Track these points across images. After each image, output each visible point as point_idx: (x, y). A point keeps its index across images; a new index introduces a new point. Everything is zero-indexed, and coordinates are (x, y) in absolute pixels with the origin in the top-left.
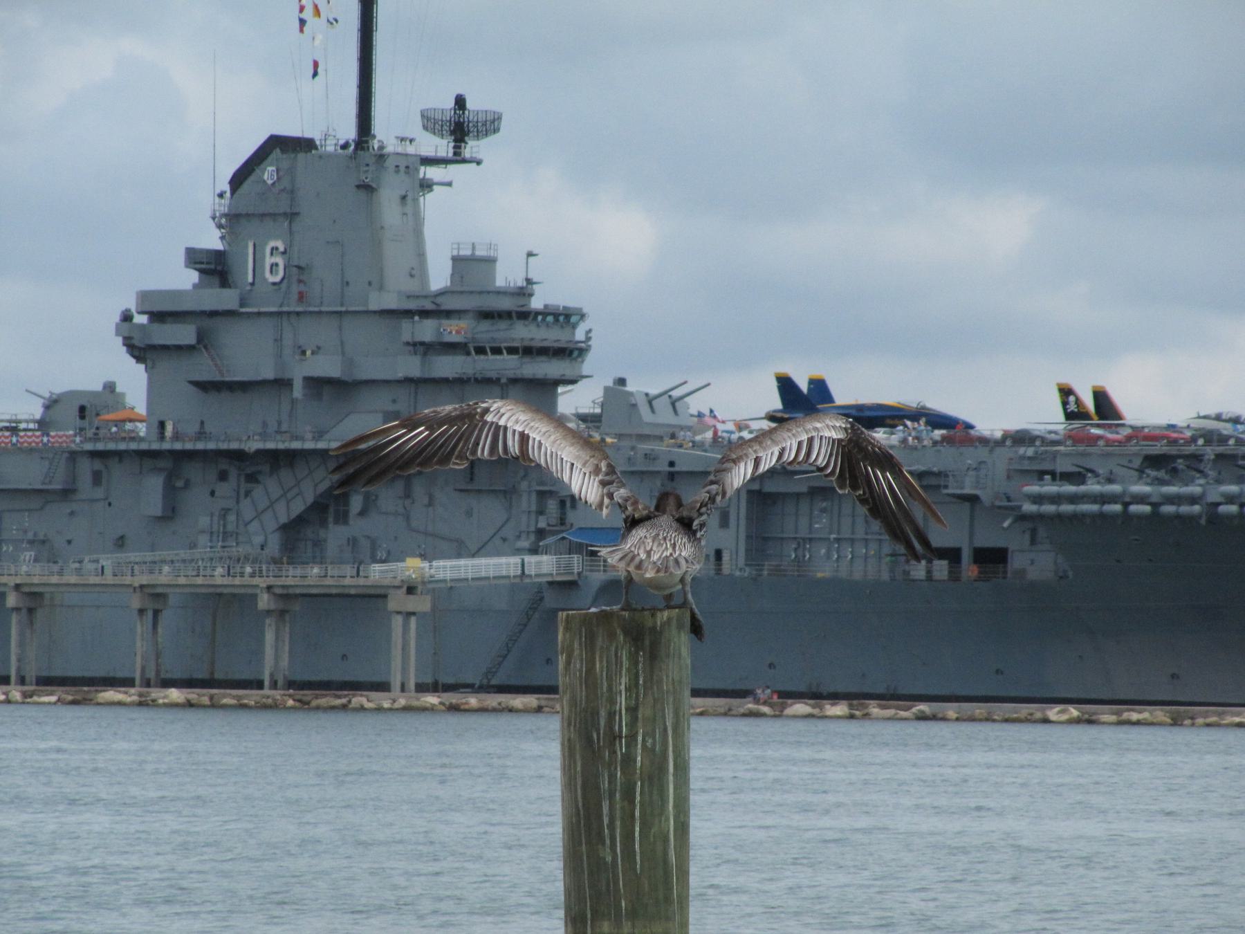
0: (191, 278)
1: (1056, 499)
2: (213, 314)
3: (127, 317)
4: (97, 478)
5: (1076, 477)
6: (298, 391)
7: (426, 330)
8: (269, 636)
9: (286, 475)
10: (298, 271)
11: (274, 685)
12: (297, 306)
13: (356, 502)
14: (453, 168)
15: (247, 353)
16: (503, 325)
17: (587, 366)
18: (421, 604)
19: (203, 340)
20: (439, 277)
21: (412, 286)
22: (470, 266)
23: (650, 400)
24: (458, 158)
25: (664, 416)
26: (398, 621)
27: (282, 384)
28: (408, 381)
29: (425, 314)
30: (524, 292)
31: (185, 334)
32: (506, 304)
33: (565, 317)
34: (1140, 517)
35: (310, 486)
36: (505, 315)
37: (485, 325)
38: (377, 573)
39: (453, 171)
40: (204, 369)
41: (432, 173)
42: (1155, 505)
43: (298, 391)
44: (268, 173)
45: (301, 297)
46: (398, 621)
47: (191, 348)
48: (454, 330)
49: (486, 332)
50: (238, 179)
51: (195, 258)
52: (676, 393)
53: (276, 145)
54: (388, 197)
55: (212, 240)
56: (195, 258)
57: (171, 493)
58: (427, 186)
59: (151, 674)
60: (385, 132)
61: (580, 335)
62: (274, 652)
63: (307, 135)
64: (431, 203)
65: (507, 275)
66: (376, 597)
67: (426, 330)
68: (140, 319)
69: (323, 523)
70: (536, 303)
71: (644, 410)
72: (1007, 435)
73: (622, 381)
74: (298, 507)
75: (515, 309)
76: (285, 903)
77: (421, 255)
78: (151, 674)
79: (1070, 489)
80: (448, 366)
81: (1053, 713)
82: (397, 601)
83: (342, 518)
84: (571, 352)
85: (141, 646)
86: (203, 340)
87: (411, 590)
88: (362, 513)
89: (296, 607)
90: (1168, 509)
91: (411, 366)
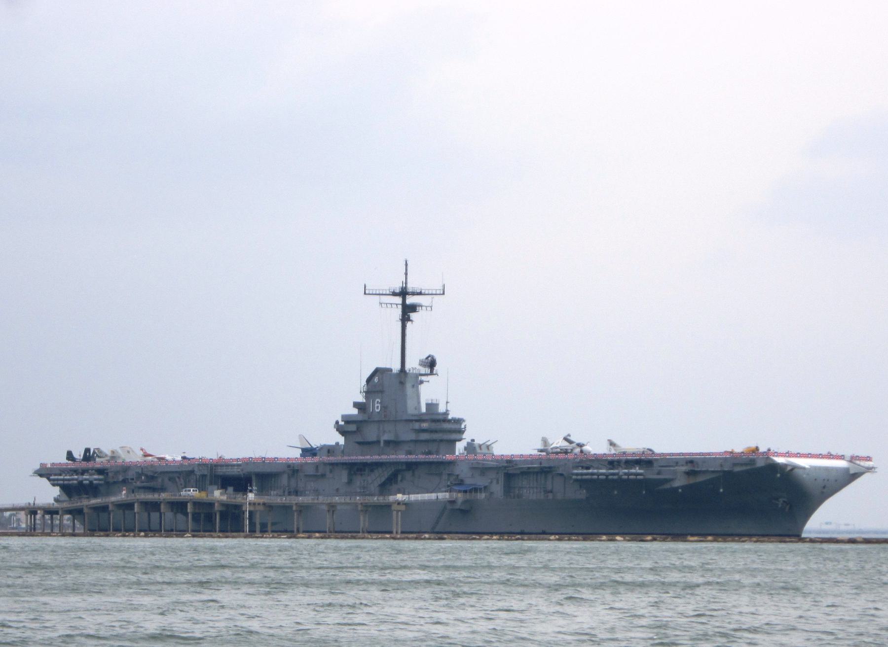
0: (355, 411)
1: (582, 474)
2: (361, 422)
3: (337, 422)
4: (331, 471)
5: (588, 468)
6: (382, 444)
7: (417, 426)
8: (362, 518)
9: (380, 469)
10: (384, 408)
11: (363, 532)
12: (383, 420)
13: (399, 478)
14: (430, 377)
15: (371, 433)
16: (438, 424)
17: (464, 436)
18: (403, 508)
19: (358, 430)
20: (424, 409)
21: (416, 412)
22: (431, 406)
23: (480, 446)
24: (432, 373)
25: (484, 450)
26: (395, 513)
27: (378, 442)
28: (412, 441)
29: (417, 421)
30: (446, 413)
31: (353, 428)
32: (441, 417)
33: (459, 421)
34: (602, 480)
35: (385, 474)
36: (438, 421)
37: (433, 424)
38: (391, 498)
39: (430, 378)
40: (360, 439)
41: (424, 378)
42: (607, 476)
43: (382, 444)
44: (376, 379)
45: (385, 416)
46: (395, 513)
47: (354, 432)
48: (425, 425)
49: (434, 426)
50: (369, 380)
51: (356, 405)
52: (488, 443)
53: (377, 371)
54: (408, 386)
55: (361, 399)
56: (356, 405)
57: (350, 475)
58: (422, 382)
59: (332, 530)
60: (408, 367)
61: (463, 426)
62: (363, 522)
63: (388, 366)
64: (423, 388)
65: (442, 409)
66: (388, 506)
67: (417, 426)
68: (343, 423)
69: (391, 485)
70: (450, 417)
71: (478, 450)
72: (322, 448)
73: (473, 440)
74: (383, 479)
75: (444, 419)
76: (69, 611)
77: (419, 403)
78: (332, 530)
79: (585, 471)
80: (424, 436)
81: (552, 537)
82: (395, 507)
83: (396, 482)
84: (461, 432)
85: (328, 521)
86: (358, 430)
87: (399, 504)
88: (401, 481)
89: (370, 509)
90: (610, 477)
91: (412, 436)
